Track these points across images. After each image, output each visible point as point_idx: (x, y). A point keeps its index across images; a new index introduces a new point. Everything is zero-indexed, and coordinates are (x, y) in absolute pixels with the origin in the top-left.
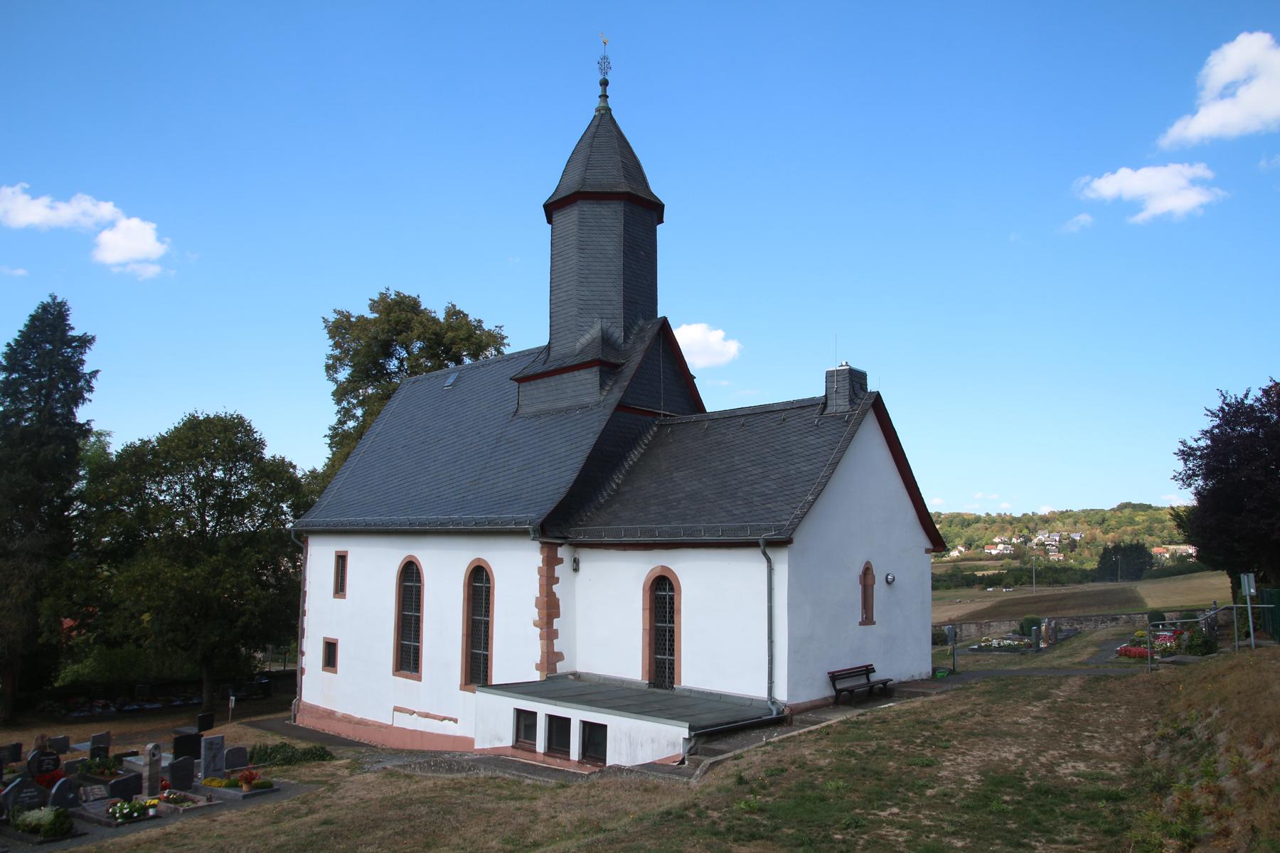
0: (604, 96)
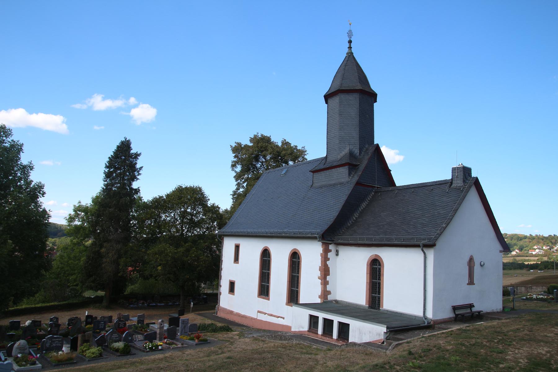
0: (350, 48)
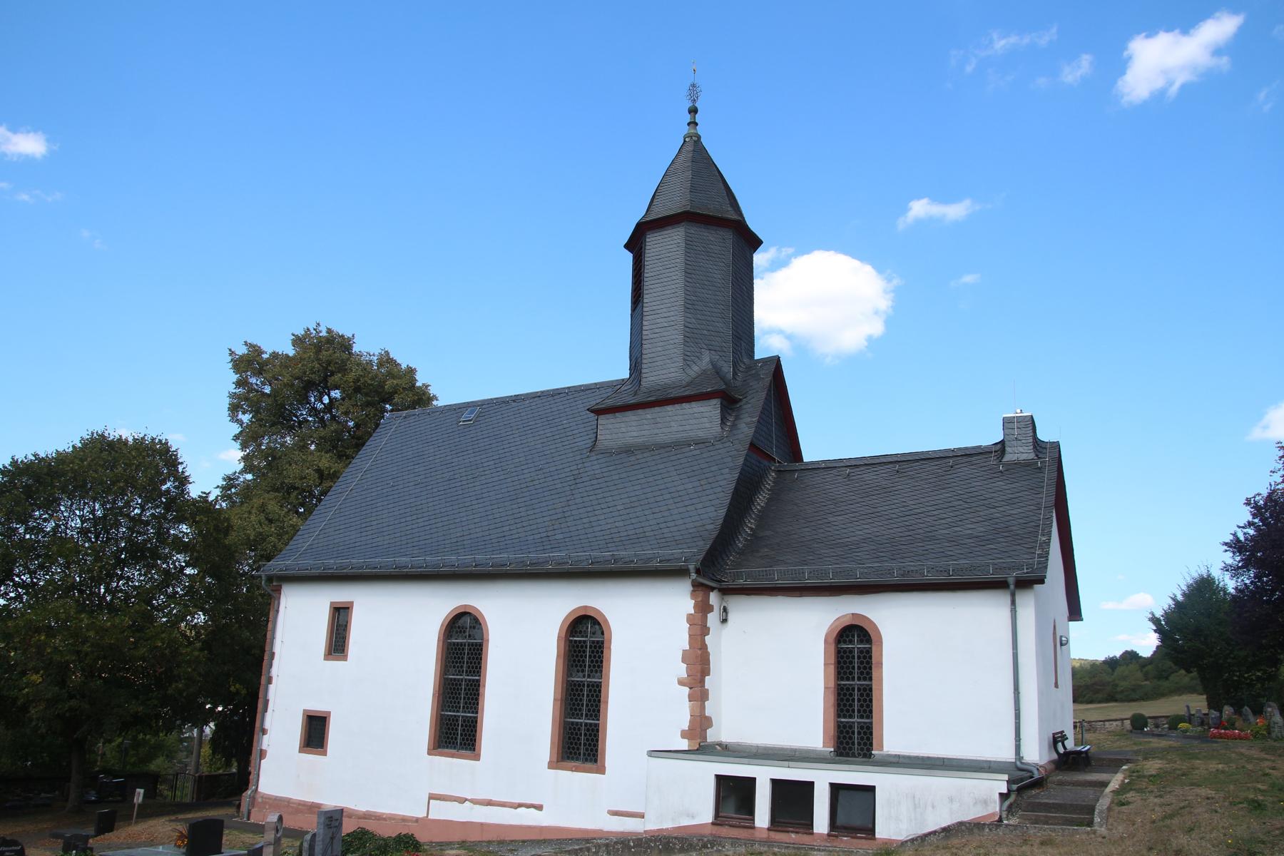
0: (693, 123)
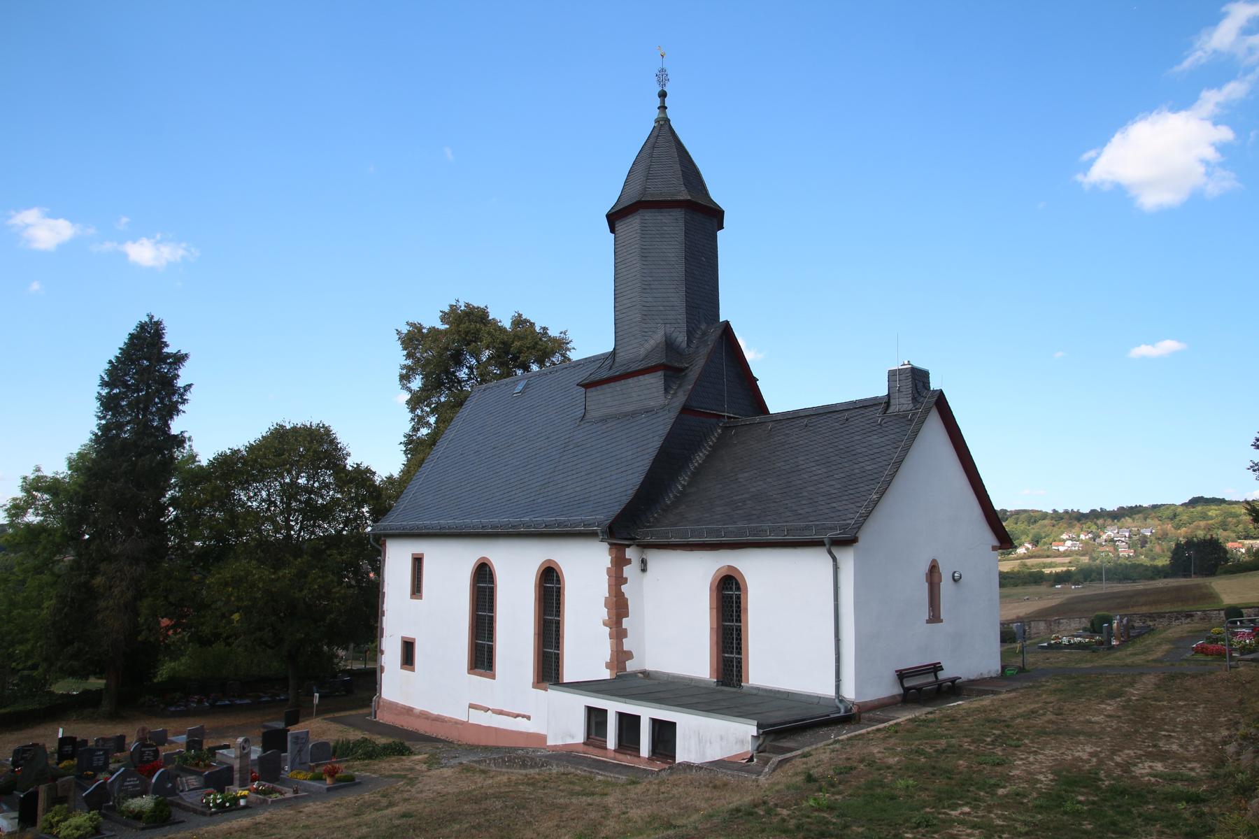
0: (663, 108)
